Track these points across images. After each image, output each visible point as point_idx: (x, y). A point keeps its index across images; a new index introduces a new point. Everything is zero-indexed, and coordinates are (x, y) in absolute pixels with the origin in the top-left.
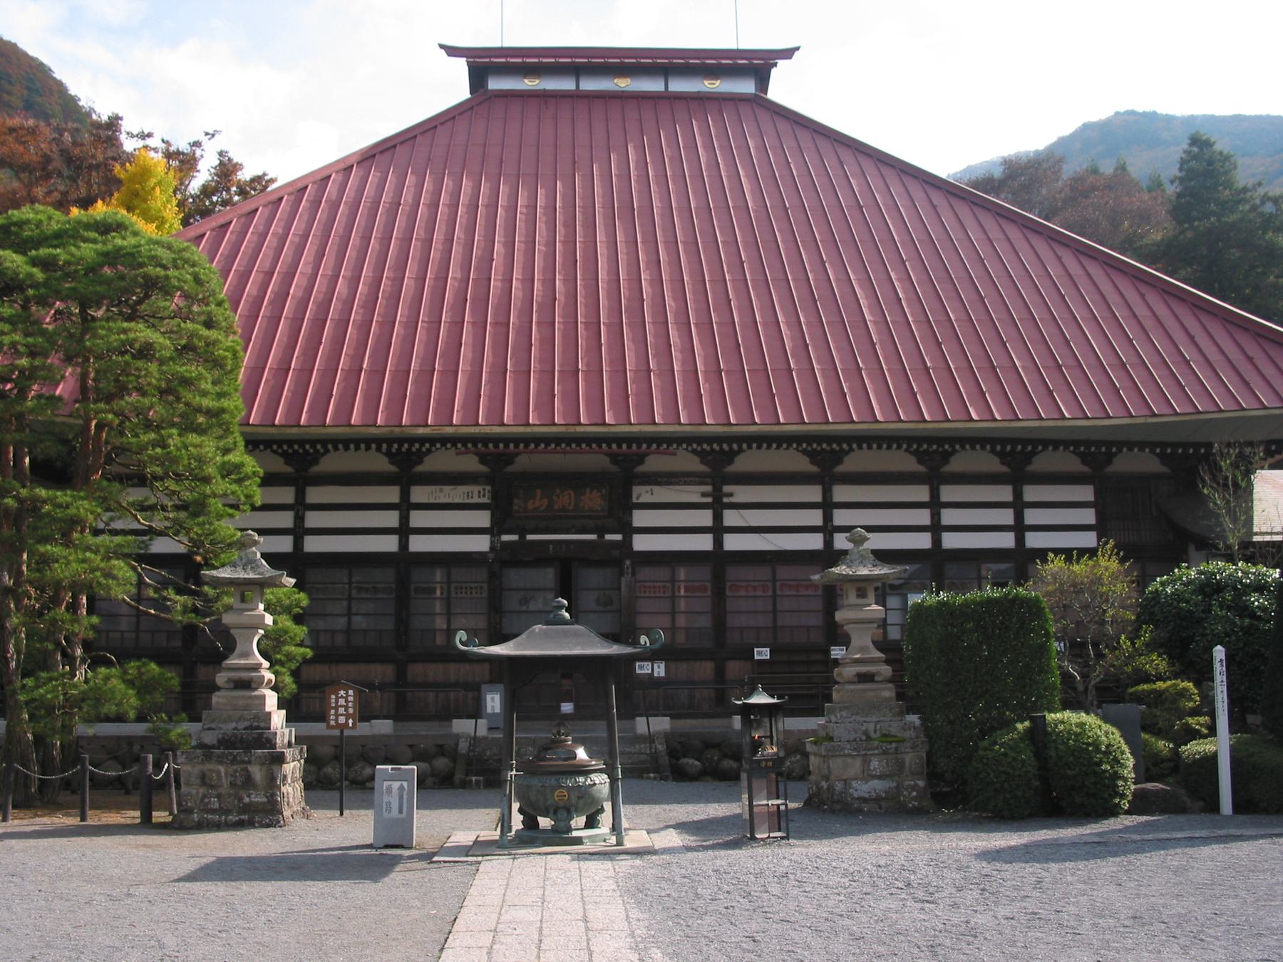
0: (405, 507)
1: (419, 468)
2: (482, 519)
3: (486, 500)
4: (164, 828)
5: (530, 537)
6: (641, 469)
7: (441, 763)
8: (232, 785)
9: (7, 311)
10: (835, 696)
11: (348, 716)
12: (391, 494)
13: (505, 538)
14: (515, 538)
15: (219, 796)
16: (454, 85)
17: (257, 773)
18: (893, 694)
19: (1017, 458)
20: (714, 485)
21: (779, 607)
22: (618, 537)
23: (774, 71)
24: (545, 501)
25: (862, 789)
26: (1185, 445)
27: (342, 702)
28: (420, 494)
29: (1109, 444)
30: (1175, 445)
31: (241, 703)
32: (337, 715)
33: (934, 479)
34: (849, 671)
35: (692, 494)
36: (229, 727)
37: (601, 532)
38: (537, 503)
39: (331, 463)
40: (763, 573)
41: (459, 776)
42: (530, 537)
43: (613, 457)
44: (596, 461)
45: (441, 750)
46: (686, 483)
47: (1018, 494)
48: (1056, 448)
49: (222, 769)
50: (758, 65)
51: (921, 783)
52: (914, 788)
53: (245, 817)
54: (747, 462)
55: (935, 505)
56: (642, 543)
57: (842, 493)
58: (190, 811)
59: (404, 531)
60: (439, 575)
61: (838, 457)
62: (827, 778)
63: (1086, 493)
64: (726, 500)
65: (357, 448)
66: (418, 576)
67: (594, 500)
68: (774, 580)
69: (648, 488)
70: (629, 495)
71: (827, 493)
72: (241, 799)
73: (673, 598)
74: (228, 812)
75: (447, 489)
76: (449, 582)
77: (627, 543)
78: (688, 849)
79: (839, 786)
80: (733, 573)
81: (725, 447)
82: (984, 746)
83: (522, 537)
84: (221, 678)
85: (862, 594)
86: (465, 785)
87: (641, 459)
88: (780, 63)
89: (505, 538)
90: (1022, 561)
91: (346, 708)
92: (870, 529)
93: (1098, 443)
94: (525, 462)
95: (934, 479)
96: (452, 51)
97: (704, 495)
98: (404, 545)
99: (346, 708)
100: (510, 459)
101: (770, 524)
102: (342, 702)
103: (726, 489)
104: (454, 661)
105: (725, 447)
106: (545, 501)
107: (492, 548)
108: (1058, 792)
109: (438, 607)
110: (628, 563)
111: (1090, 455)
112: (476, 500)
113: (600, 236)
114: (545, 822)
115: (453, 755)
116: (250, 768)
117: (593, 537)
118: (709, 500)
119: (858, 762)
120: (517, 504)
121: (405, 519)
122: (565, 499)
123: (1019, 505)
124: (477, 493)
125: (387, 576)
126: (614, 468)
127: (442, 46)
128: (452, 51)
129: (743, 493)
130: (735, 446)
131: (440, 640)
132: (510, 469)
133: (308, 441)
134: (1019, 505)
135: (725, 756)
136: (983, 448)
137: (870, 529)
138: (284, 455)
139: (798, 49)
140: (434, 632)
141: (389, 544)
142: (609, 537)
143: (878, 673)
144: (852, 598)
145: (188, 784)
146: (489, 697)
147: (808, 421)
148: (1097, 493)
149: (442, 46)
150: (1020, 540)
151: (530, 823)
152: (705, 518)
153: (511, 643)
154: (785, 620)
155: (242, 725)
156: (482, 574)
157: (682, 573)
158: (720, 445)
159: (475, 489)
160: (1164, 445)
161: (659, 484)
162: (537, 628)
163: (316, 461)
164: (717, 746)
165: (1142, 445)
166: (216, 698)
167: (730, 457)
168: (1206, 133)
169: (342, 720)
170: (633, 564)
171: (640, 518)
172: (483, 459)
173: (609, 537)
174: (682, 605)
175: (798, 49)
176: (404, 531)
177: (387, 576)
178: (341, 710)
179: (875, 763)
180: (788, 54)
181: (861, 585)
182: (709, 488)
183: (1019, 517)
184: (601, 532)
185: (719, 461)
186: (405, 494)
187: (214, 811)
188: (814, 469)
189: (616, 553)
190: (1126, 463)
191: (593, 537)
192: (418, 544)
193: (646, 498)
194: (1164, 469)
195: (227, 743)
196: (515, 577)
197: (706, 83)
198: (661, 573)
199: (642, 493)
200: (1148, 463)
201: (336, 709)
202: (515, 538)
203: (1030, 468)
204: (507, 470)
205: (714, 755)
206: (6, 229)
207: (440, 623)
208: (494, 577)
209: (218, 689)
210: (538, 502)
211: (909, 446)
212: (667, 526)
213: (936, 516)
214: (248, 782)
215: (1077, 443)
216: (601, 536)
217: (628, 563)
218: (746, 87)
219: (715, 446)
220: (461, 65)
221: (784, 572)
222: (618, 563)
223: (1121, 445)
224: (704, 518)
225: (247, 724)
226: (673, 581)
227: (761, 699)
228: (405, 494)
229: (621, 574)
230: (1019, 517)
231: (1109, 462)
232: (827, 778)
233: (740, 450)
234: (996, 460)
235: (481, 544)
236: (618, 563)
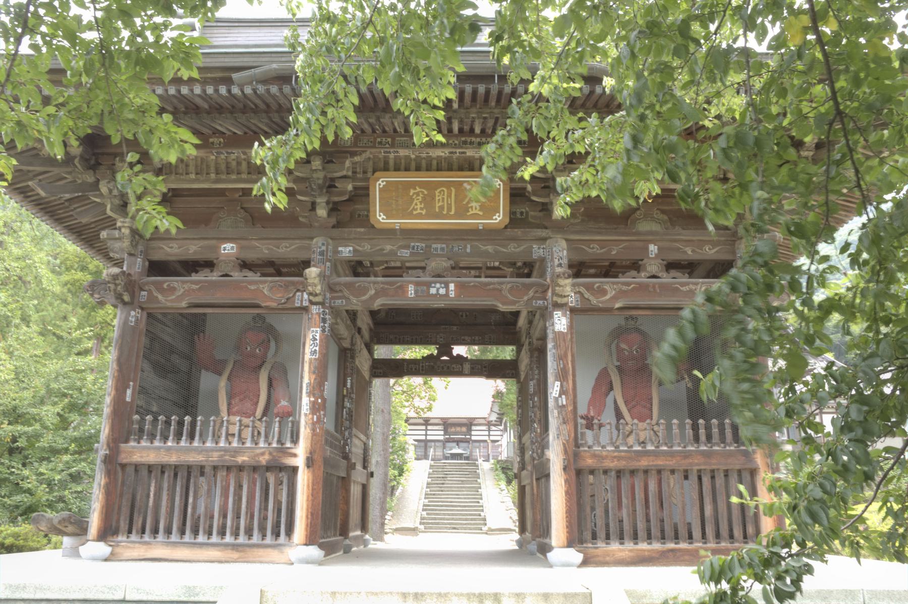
0: (426, 430)
2: (442, 433)
9: (540, 2)
12: (424, 428)
28: (429, 427)
44: (465, 421)
56: (473, 438)
66: (429, 444)
67: (464, 429)
78: (867, 507)
80: (429, 444)
94: (450, 421)
113: (164, 503)
122: (458, 429)
124: (441, 427)
125: (423, 444)
171: (473, 433)
192: (429, 438)
199: (474, 428)
206: (68, 2)
210: (453, 430)
224: (487, 433)
235: (442, 438)
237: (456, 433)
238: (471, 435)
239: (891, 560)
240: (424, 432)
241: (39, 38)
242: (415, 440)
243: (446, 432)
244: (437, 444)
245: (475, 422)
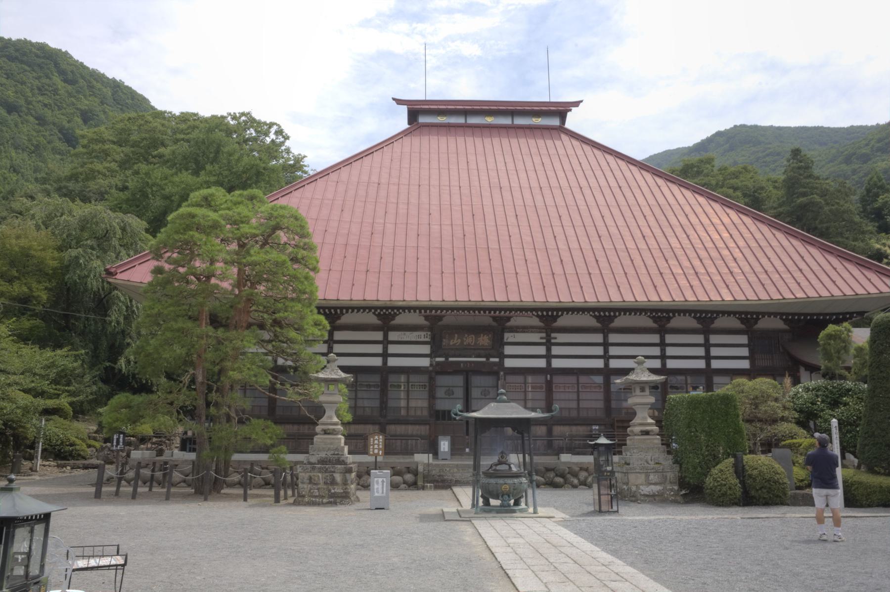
0: (386, 342)
1: (555, 324)
3: (428, 340)
4: (290, 504)
5: (451, 359)
6: (509, 324)
7: (409, 477)
8: (325, 483)
10: (628, 442)
11: (379, 449)
13: (438, 359)
14: (442, 359)
15: (318, 489)
16: (401, 122)
17: (338, 477)
18: (660, 442)
19: (706, 319)
20: (546, 333)
21: (581, 398)
22: (497, 360)
23: (569, 114)
24: (459, 341)
25: (646, 490)
26: (799, 315)
27: (376, 442)
29: (712, 312)
30: (793, 314)
31: (328, 441)
32: (374, 449)
33: (662, 331)
34: (637, 429)
35: (535, 337)
36: (323, 455)
37: (488, 357)
38: (455, 341)
39: (621, 321)
40: (572, 379)
41: (420, 483)
42: (451, 359)
43: (494, 319)
44: (485, 319)
45: (409, 470)
46: (532, 332)
47: (662, 339)
48: (583, 312)
49: (320, 475)
50: (561, 111)
51: (676, 488)
52: (672, 490)
53: (332, 500)
54: (564, 321)
55: (606, 345)
56: (509, 363)
57: (613, 338)
58: (304, 496)
59: (385, 355)
60: (403, 378)
61: (611, 319)
62: (627, 484)
63: (743, 339)
64: (553, 341)
65: (415, 312)
66: (392, 378)
67: (485, 340)
68: (578, 383)
69: (512, 334)
70: (503, 338)
71: (606, 338)
72: (330, 491)
73: (525, 392)
74: (323, 497)
75: (408, 333)
76: (408, 382)
77: (501, 363)
79: (634, 488)
80: (392, 378)
81: (602, 314)
82: (714, 467)
83: (447, 359)
84: (318, 429)
85: (643, 390)
86: (423, 488)
87: (508, 319)
88: (573, 109)
89: (438, 359)
90: (708, 376)
91: (378, 445)
92: (647, 357)
93: (752, 313)
94: (449, 319)
95: (662, 331)
96: (399, 102)
97: (541, 338)
98: (385, 362)
99: (378, 445)
100: (440, 318)
101: (576, 354)
102: (376, 442)
103: (553, 335)
104: (411, 424)
105: (607, 314)
106: (459, 341)
107: (431, 365)
108: (755, 494)
109: (403, 395)
110: (502, 373)
111: (747, 318)
112: (423, 339)
114: (494, 502)
115: (416, 473)
116: (335, 475)
117: (484, 359)
118: (544, 341)
119: (643, 476)
120: (445, 342)
121: (385, 349)
122: (470, 340)
123: (707, 346)
124: (423, 336)
125: (376, 379)
126: (494, 324)
127: (394, 99)
128: (399, 102)
129: (561, 338)
130: (612, 314)
131: (403, 412)
132: (440, 323)
133: (333, 308)
134: (707, 346)
135: (557, 475)
136: (690, 315)
137: (647, 357)
138: (653, 318)
139: (582, 101)
140: (399, 408)
141: (377, 362)
142: (492, 360)
143: (652, 431)
144: (638, 392)
145: (303, 483)
146: (442, 443)
147: (540, 298)
148: (750, 339)
149: (394, 99)
150: (708, 364)
151: (487, 503)
152: (542, 350)
153: (481, 412)
154: (583, 404)
155: (329, 453)
156: (424, 378)
157: (530, 379)
158: (604, 313)
159: (422, 333)
160: (787, 314)
161: (517, 332)
162: (492, 404)
163: (339, 318)
164: (553, 470)
165: (729, 313)
166: (316, 439)
167: (555, 319)
168: (811, 152)
169: (376, 451)
170: (505, 374)
172: (427, 318)
173: (492, 360)
174: (530, 396)
175: (582, 101)
176: (385, 355)
177: (376, 379)
178: (376, 446)
179: (652, 477)
180: (576, 104)
181: (642, 385)
182: (544, 335)
183: (708, 352)
184: (488, 357)
185: (549, 319)
186: (386, 336)
187: (316, 497)
188: (655, 325)
189: (496, 368)
190: (764, 324)
191: (484, 359)
192: (392, 362)
193: (511, 340)
194: (786, 327)
195: (322, 462)
196: (442, 380)
197: (534, 119)
198: (519, 379)
199: (509, 337)
200: (778, 324)
201: (373, 445)
202: (442, 359)
203: (713, 326)
204: (438, 322)
205: (551, 475)
207: (403, 403)
208: (431, 379)
209: (317, 434)
210: (455, 341)
211: (696, 314)
212: (522, 353)
213: (663, 351)
214: (333, 482)
215: (740, 313)
216: (488, 359)
217: (502, 373)
218: (555, 122)
219: (602, 314)
220: (404, 109)
221: (583, 379)
222: (496, 373)
223: (764, 314)
225: (332, 452)
226: (525, 383)
227: (603, 440)
228: (386, 336)
229: (498, 379)
230: (708, 352)
231: (756, 323)
232: (627, 484)
233: (615, 317)
234: (375, 317)
235: (425, 362)
236: (496, 373)
237: (463, 351)
238: (502, 356)
239: (10, 40)
240: (599, 351)
241: (114, 166)
242: (344, 369)
243: (437, 348)
244: (414, 378)
245: (512, 323)
